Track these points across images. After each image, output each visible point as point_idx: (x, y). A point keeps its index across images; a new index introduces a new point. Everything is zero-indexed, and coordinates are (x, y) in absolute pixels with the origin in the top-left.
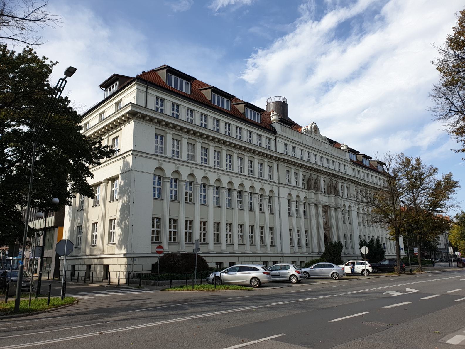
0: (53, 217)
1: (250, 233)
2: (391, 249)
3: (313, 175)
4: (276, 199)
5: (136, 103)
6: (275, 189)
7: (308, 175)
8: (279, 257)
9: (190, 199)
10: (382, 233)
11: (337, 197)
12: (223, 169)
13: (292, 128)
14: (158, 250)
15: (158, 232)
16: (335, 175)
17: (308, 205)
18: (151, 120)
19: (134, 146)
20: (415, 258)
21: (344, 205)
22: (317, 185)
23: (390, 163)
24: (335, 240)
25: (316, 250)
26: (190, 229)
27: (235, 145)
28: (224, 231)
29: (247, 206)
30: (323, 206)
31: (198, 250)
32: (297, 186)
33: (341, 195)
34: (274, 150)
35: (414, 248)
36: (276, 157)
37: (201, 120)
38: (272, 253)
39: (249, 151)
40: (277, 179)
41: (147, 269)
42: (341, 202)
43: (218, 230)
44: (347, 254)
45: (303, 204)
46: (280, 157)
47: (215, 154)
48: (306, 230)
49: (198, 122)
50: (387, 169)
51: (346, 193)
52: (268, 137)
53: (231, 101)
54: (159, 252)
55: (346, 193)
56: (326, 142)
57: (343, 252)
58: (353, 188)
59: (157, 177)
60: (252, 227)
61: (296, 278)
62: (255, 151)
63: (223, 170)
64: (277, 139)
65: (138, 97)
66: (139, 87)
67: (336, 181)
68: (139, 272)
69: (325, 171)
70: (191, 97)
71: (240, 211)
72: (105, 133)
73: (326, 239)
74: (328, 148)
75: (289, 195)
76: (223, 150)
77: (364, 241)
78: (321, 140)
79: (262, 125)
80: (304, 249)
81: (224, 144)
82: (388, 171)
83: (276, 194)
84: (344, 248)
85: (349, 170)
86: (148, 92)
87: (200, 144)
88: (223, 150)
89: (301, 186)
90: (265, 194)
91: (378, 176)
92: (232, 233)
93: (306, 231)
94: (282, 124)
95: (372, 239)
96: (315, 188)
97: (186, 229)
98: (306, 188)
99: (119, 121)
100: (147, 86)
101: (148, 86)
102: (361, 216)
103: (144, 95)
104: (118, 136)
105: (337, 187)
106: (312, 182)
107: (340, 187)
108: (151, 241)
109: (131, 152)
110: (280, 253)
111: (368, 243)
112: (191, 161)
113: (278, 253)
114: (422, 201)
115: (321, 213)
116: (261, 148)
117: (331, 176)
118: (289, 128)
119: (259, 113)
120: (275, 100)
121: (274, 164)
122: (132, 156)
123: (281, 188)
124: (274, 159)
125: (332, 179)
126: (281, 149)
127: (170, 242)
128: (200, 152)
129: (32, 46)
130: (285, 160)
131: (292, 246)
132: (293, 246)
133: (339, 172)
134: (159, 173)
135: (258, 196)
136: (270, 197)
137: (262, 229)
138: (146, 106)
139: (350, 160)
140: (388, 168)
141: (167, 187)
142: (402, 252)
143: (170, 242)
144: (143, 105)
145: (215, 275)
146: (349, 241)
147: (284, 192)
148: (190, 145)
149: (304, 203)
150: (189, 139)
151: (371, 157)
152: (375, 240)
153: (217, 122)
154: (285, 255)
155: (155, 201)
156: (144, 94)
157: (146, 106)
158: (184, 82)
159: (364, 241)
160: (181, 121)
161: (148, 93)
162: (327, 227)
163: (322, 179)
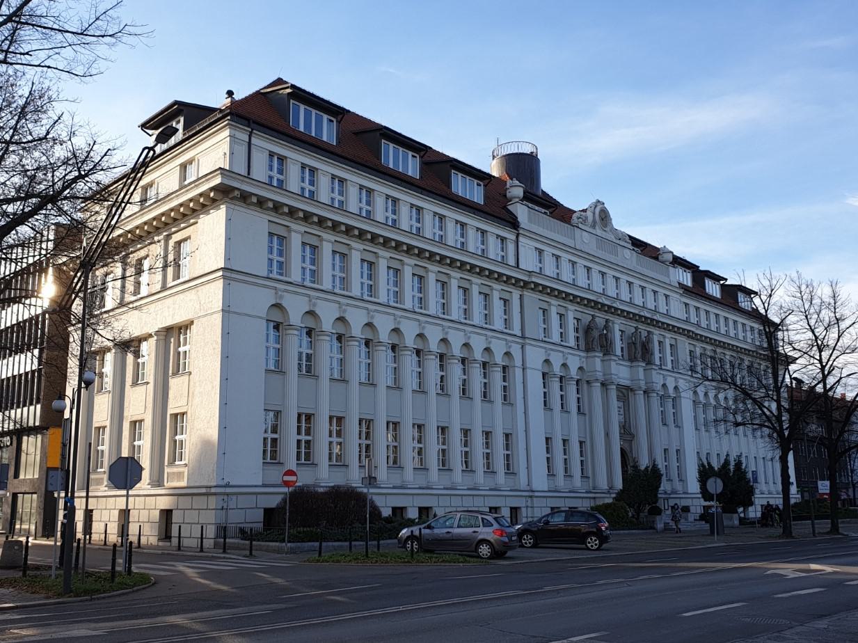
0: (39, 406)
1: (461, 446)
2: (766, 483)
3: (597, 319)
4: (519, 372)
5: (228, 168)
6: (516, 351)
7: (586, 319)
8: (524, 499)
9: (308, 367)
10: (756, 452)
11: (649, 367)
12: (474, 324)
13: (551, 213)
14: (287, 478)
15: (274, 441)
16: (646, 318)
17: (585, 386)
18: (261, 202)
19: (227, 259)
20: (820, 504)
21: (664, 385)
22: (606, 340)
23: (770, 296)
24: (644, 463)
25: (603, 483)
26: (308, 433)
27: (410, 248)
28: (382, 438)
29: (410, 382)
30: (620, 388)
31: (372, 480)
32: (562, 343)
33: (658, 362)
34: (514, 265)
35: (820, 483)
36: (518, 280)
37: (271, 169)
38: (509, 489)
39: (439, 262)
40: (520, 328)
41: (256, 519)
42: (657, 379)
43: (368, 436)
44: (668, 492)
45: (558, 379)
46: (526, 279)
47: (362, 268)
48: (582, 440)
49: (353, 206)
50: (765, 308)
51: (669, 358)
52: (500, 236)
53: (421, 157)
54: (287, 484)
55: (669, 358)
56: (626, 245)
57: (662, 488)
58: (685, 345)
59: (272, 325)
60: (466, 432)
61: (481, 546)
62: (453, 261)
63: (405, 310)
64: (521, 239)
65: (232, 154)
66: (233, 132)
67: (648, 332)
68: (240, 525)
69: (721, 342)
70: (339, 151)
71: (440, 397)
72: (157, 228)
73: (624, 457)
74: (629, 257)
75: (486, 352)
76: (353, 251)
77: (709, 464)
78: (614, 240)
79: (487, 209)
80: (577, 481)
81: (372, 242)
82: (766, 311)
83: (518, 362)
84: (664, 478)
85: (677, 308)
86: (252, 142)
87: (300, 236)
88: (353, 251)
89: (572, 343)
90: (379, 338)
91: (740, 320)
92: (471, 448)
93: (581, 443)
94: (530, 205)
95: (725, 460)
96: (601, 347)
97: (299, 433)
98: (582, 346)
99: (191, 205)
100: (250, 130)
101: (252, 130)
102: (700, 410)
103: (244, 148)
104: (189, 238)
105: (650, 345)
106: (596, 334)
107: (656, 344)
108: (262, 461)
109: (220, 273)
110: (526, 489)
111: (716, 469)
112: (353, 294)
113: (522, 489)
114: (841, 378)
115: (615, 404)
116: (466, 253)
117: (636, 320)
118: (545, 213)
119: (334, 120)
120: (509, 150)
121: (514, 295)
122: (222, 280)
123: (528, 348)
124: (514, 285)
125: (639, 327)
126: (529, 261)
127: (300, 462)
128: (300, 253)
129: (82, 78)
130: (537, 285)
131: (551, 474)
132: (571, 476)
133: (656, 311)
134: (278, 317)
135: (478, 365)
136: (504, 368)
137: (466, 435)
138: (249, 174)
139: (677, 286)
140: (766, 305)
141: (295, 345)
142: (793, 489)
143: (300, 462)
144: (244, 172)
145: (412, 532)
146: (674, 464)
147: (535, 356)
148: (416, 277)
149: (578, 381)
150: (365, 252)
151: (725, 277)
152: (733, 463)
153: (310, 176)
154: (536, 494)
155: (362, 387)
156: (265, 154)
157: (249, 174)
158: (325, 117)
159: (709, 464)
160: (287, 193)
161: (252, 146)
162: (627, 432)
163: (618, 325)
